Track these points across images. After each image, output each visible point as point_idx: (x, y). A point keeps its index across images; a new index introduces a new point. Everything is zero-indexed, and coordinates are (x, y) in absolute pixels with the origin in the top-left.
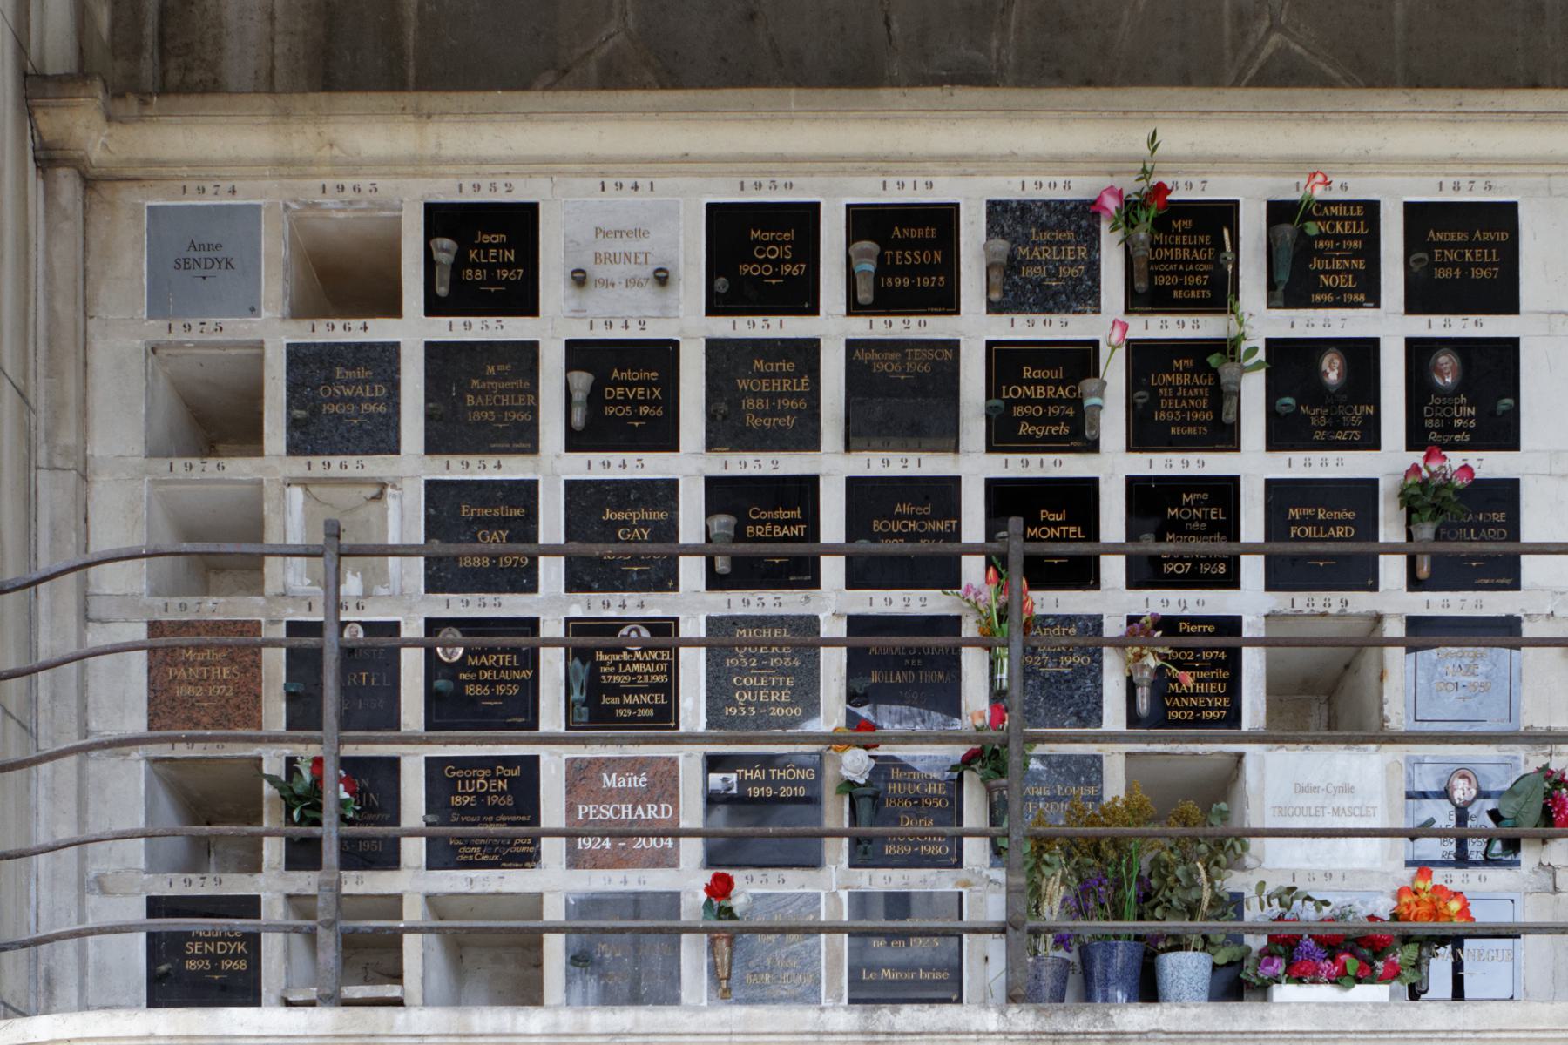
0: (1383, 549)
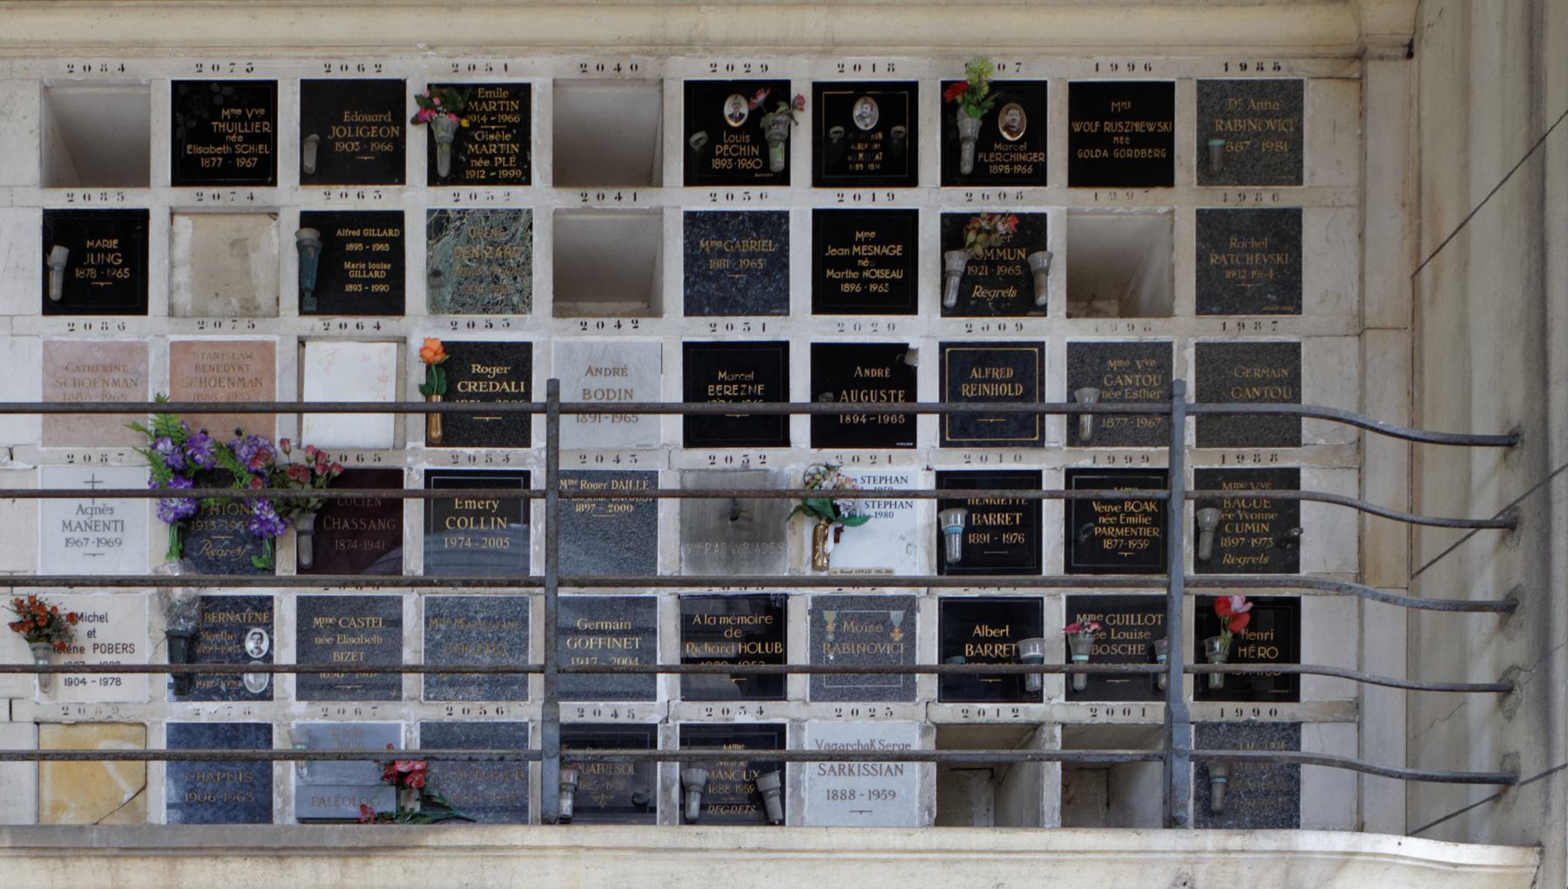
0: (794, 409)
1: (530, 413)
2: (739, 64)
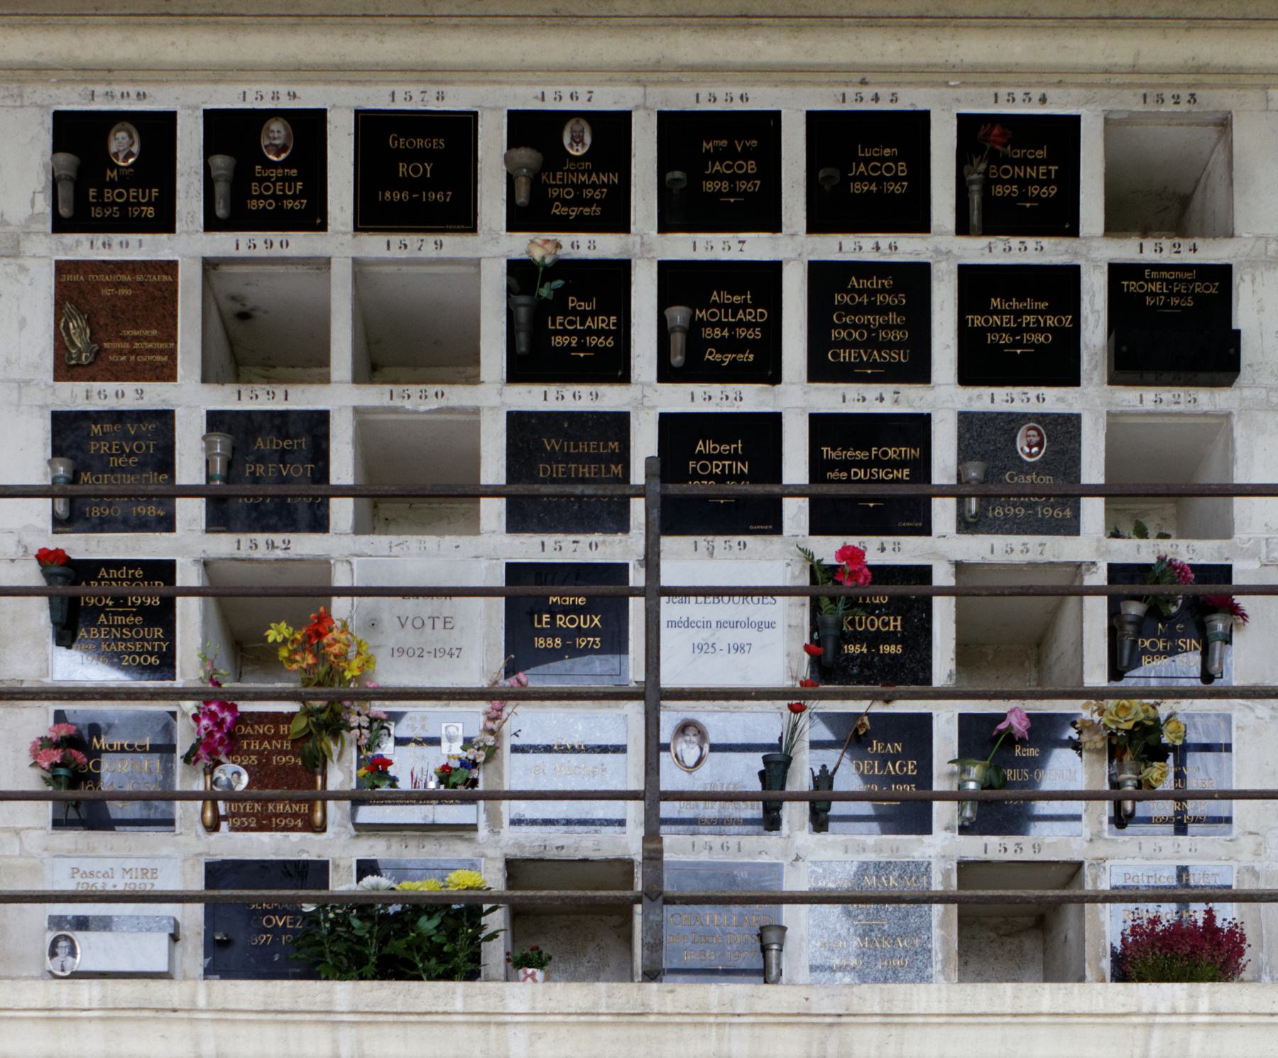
1: (328, 497)
2: (550, 91)
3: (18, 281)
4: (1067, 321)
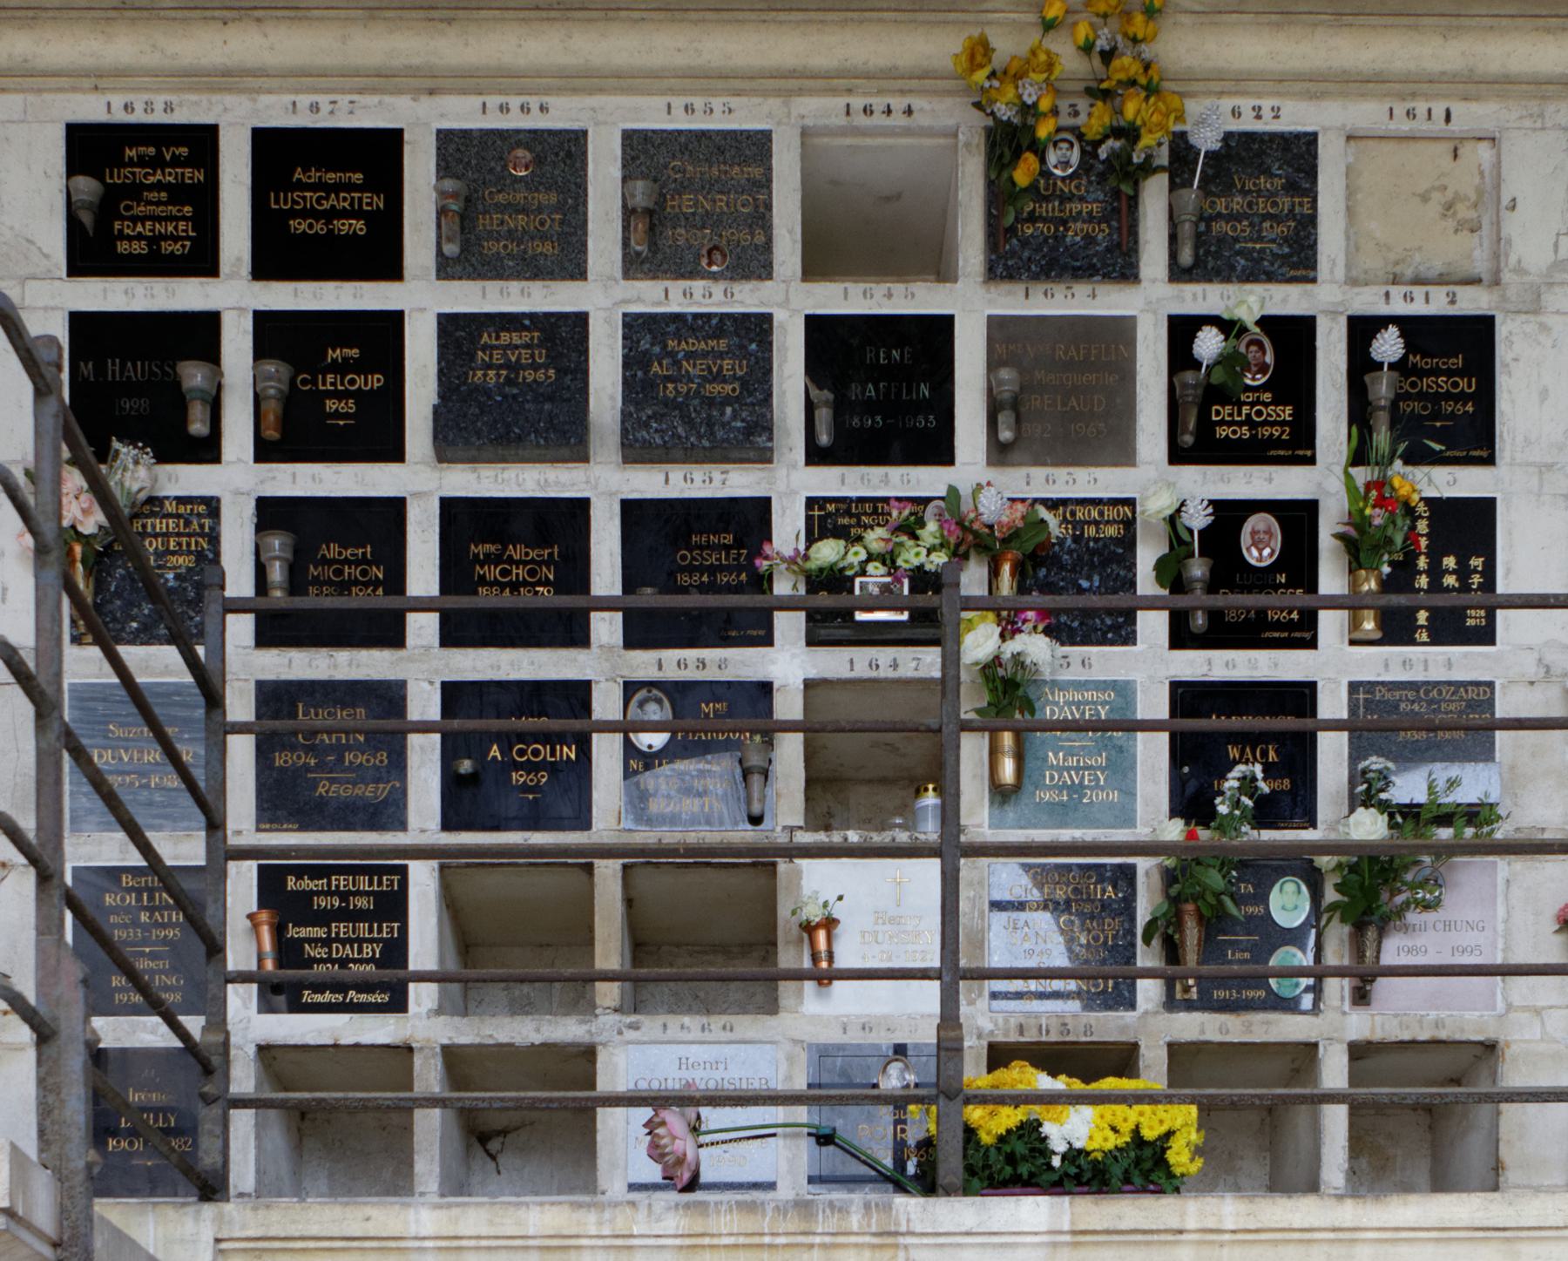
2: (139, 101)
3: (1539, 344)
4: (376, 381)
